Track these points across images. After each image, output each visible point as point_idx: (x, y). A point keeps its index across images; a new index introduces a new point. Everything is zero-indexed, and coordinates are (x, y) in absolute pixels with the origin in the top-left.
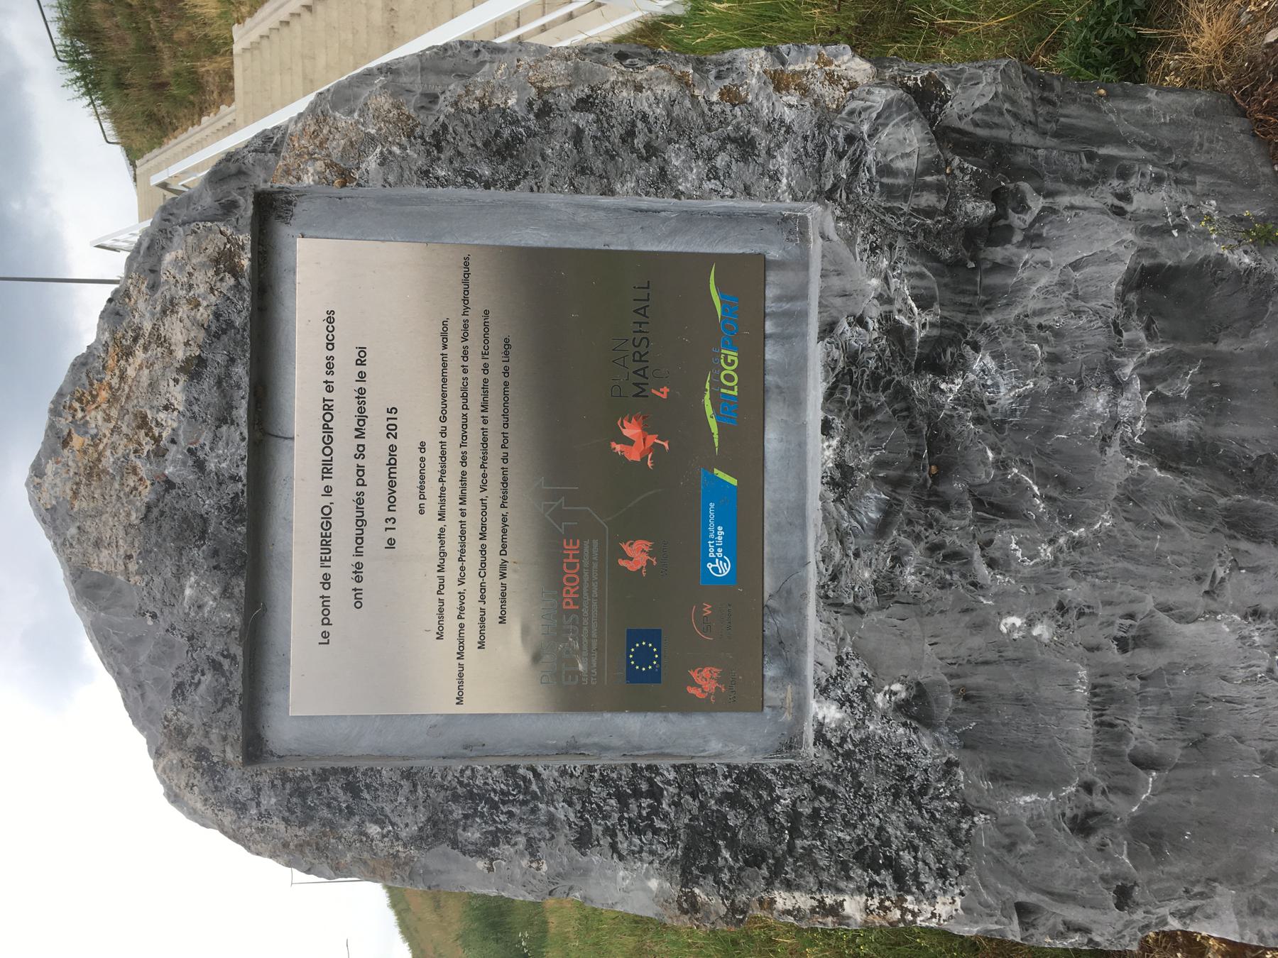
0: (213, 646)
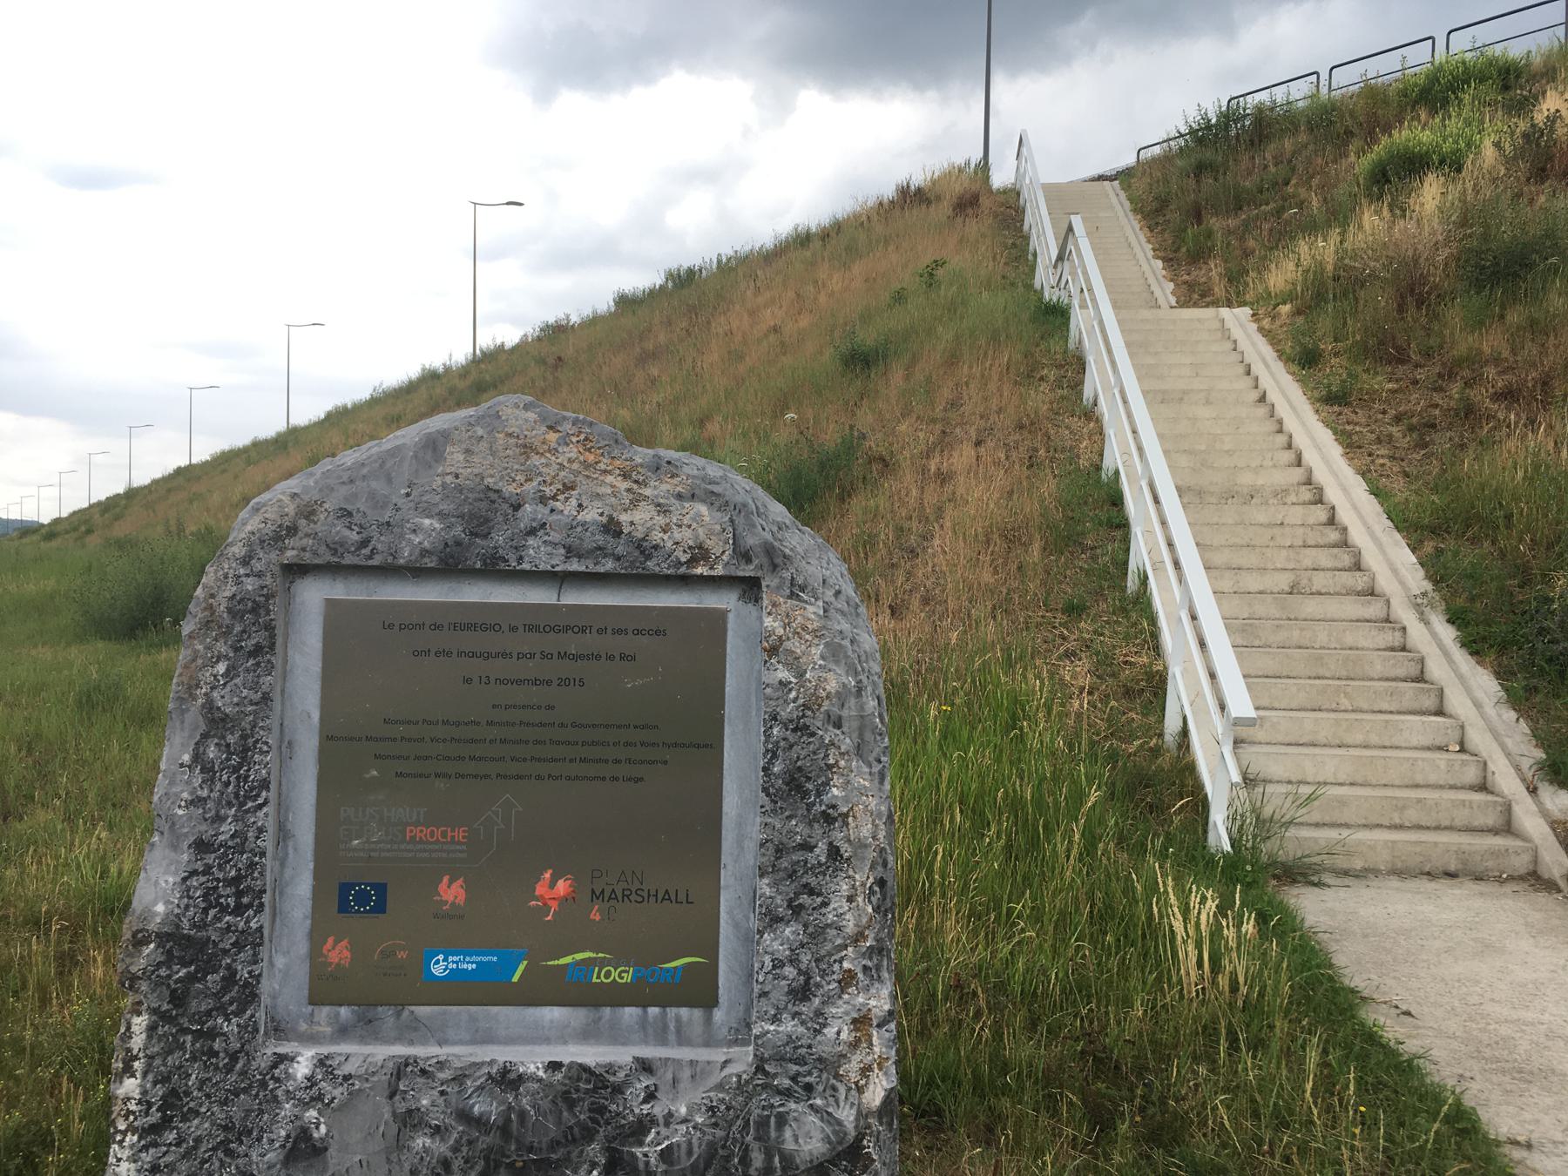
0: (380, 542)
